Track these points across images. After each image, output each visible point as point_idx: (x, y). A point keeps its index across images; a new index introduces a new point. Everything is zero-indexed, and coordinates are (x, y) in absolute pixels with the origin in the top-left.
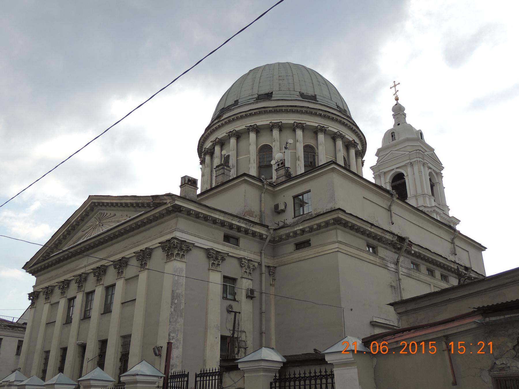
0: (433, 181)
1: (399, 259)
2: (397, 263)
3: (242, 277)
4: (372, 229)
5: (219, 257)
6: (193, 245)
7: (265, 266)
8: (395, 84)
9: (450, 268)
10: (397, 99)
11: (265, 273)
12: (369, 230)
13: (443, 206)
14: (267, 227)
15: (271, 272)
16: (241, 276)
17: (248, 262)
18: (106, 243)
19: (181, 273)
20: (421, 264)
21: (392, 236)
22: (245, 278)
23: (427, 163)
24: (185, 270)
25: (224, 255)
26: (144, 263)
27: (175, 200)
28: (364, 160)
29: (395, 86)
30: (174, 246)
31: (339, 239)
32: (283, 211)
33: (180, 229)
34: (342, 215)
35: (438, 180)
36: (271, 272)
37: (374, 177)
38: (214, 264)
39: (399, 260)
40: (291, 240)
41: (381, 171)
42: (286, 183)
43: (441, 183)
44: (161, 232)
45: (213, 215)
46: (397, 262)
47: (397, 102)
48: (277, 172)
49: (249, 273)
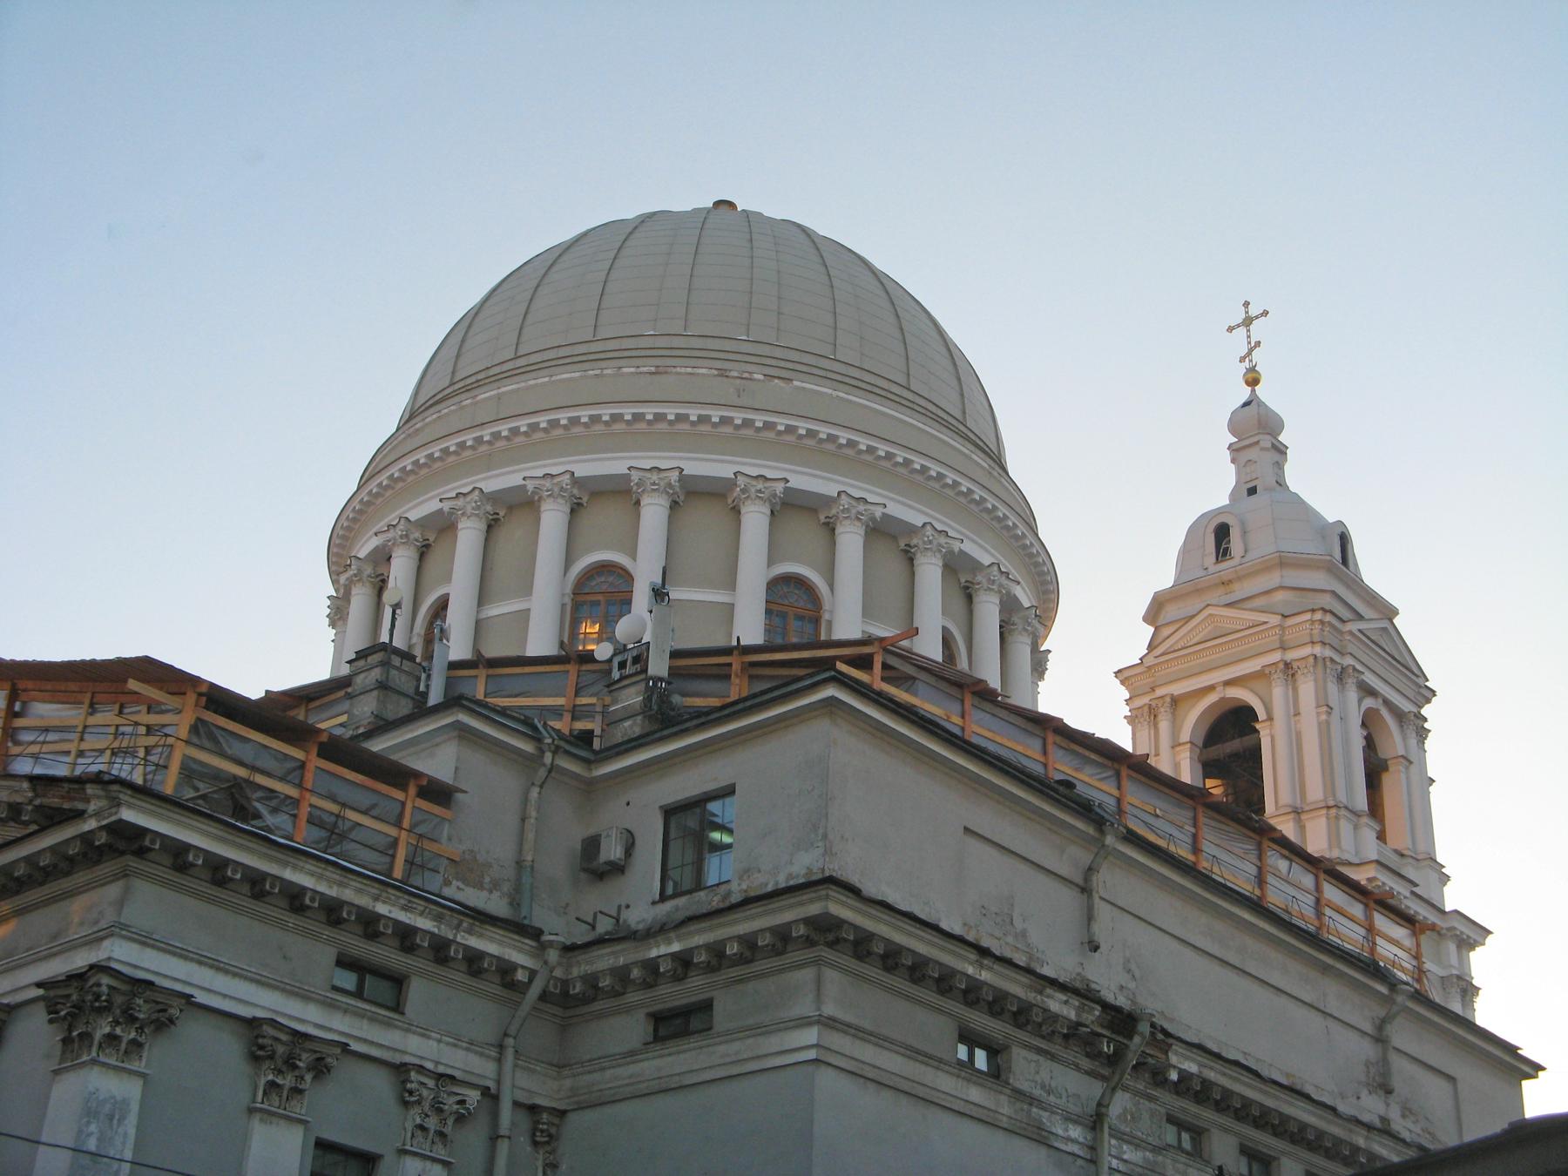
0: (1385, 752)
1: (1105, 1103)
2: (1095, 1122)
3: (403, 1152)
4: (983, 973)
5: (304, 1056)
6: (183, 1001)
7: (516, 1104)
8: (1247, 312)
9: (1347, 1153)
10: (1253, 380)
11: (509, 1138)
12: (968, 975)
13: (1418, 860)
14: (536, 934)
15: (538, 1134)
16: (399, 1145)
17: (437, 1086)
18: (64, 877)
19: (119, 1120)
20: (1213, 1130)
21: (1077, 1003)
22: (415, 1154)
23: (1355, 669)
24: (135, 1107)
25: (325, 1049)
26: (79, 1034)
27: (119, 805)
28: (1049, 651)
29: (1248, 322)
30: (97, 1004)
31: (829, 1009)
32: (617, 869)
33: (134, 930)
34: (843, 904)
35: (1406, 746)
36: (538, 1134)
37: (1129, 714)
38: (278, 1086)
39: (1103, 1110)
40: (633, 997)
41: (1159, 692)
42: (641, 750)
43: (1414, 762)
44: (55, 937)
45: (288, 874)
46: (1097, 1115)
47: (1253, 391)
48: (615, 694)
49: (435, 1132)
